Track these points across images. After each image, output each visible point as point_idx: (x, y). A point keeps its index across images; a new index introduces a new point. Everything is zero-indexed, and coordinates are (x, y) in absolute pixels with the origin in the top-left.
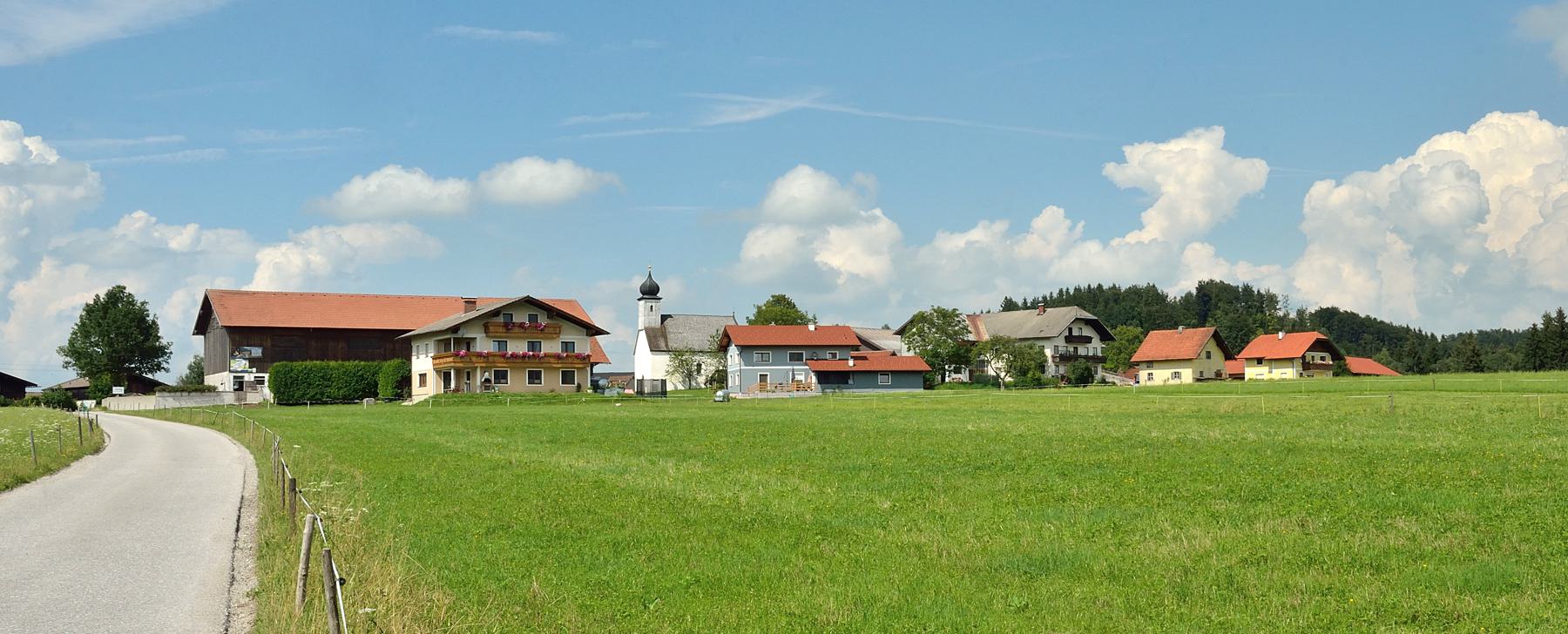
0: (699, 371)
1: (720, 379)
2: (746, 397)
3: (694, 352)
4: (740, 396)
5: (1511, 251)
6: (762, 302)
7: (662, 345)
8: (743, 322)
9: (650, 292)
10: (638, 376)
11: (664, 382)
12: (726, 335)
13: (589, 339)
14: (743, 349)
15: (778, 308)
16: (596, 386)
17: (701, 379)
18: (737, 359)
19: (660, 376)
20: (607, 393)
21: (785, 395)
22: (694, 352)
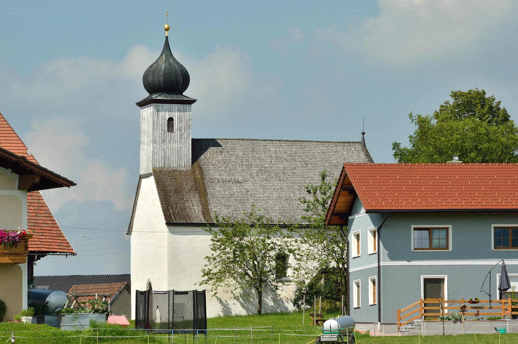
0: (281, 271)
1: (331, 290)
2: (392, 332)
3: (269, 227)
4: (377, 330)
5: (222, 315)
6: (429, 110)
7: (196, 211)
8: (384, 156)
9: (168, 86)
10: (138, 285)
11: (199, 298)
12: (346, 187)
13: (24, 198)
14: (387, 219)
15: (467, 124)
16: (40, 308)
17: (287, 292)
18: (371, 243)
19: (190, 283)
20: (68, 324)
21: (485, 328)
22: (269, 227)
